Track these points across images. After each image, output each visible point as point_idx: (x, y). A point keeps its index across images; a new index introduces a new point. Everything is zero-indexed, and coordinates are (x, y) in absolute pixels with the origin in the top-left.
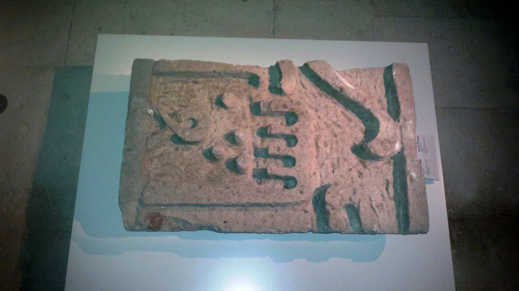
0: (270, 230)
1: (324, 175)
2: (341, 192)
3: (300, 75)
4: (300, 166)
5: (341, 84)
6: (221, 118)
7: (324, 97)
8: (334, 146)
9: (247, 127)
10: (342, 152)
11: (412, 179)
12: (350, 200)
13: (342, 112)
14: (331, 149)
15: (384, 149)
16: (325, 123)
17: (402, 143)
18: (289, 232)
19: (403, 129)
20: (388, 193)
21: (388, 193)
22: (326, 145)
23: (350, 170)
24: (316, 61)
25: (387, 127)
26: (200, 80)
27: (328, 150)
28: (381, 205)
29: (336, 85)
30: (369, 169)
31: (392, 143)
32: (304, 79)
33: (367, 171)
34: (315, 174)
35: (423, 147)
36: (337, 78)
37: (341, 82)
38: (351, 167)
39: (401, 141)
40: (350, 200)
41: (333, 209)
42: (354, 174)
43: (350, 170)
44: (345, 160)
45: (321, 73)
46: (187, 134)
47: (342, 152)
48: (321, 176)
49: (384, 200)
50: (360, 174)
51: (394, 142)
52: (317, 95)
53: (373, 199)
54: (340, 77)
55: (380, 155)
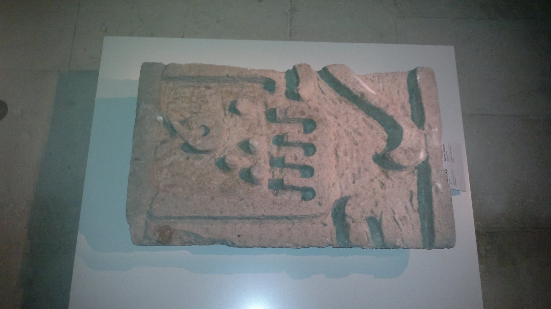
0: (287, 245)
1: (344, 186)
2: (362, 204)
3: (318, 79)
4: (319, 176)
5: (362, 89)
6: (235, 126)
7: (343, 102)
8: (355, 155)
10: (363, 161)
12: (372, 212)
13: (363, 119)
14: (351, 158)
15: (408, 158)
18: (306, 246)
19: (428, 137)
20: (412, 205)
22: (346, 154)
23: (372, 180)
24: (335, 65)
25: (411, 135)
26: (212, 85)
27: (348, 160)
28: (405, 217)
29: (356, 90)
30: (392, 179)
31: (416, 152)
33: (389, 181)
34: (334, 184)
35: (449, 156)
36: (358, 82)
37: (362, 87)
38: (373, 177)
39: (426, 149)
40: (372, 212)
41: (353, 222)
42: (376, 184)
44: (366, 169)
45: (341, 77)
46: (199, 142)
47: (363, 161)
48: (341, 187)
49: (407, 212)
50: (383, 185)
51: (419, 151)
52: (337, 101)
53: (396, 212)
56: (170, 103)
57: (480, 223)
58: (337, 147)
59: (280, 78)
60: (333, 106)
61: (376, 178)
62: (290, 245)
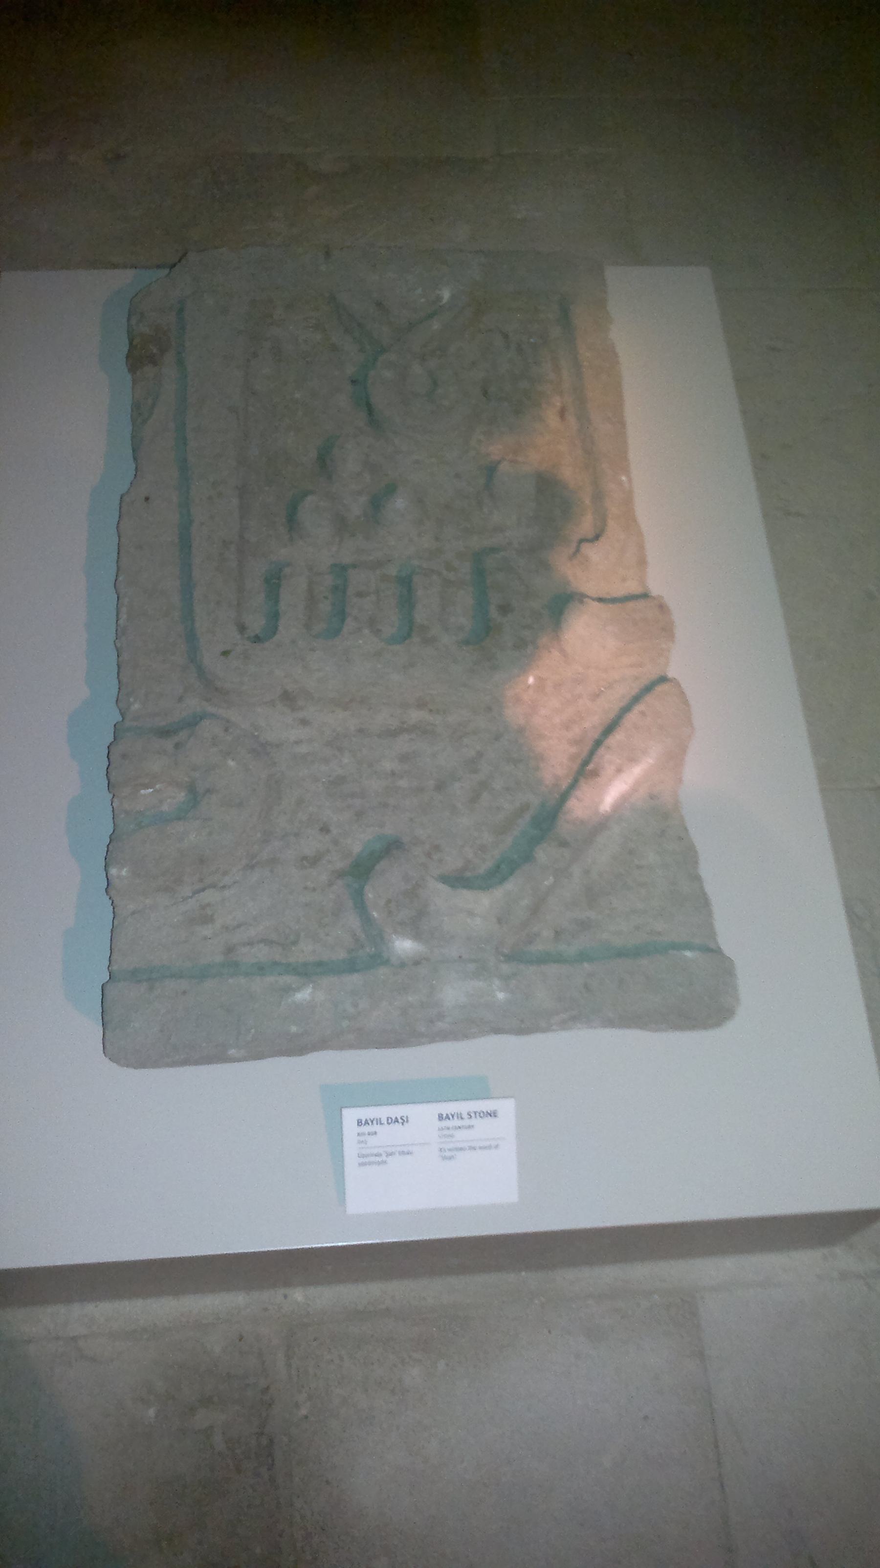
0: (124, 610)
1: (303, 749)
2: (231, 763)
3: (637, 678)
4: (313, 650)
5: (610, 770)
6: (457, 476)
7: (573, 750)
8: (403, 783)
9: (437, 539)
10: (385, 805)
11: (288, 990)
12: (208, 791)
13: (525, 808)
14: (393, 774)
15: (389, 901)
16: (480, 755)
17: (417, 963)
18: (121, 659)
19: (471, 967)
20: (250, 943)
21: (250, 943)
22: (404, 758)
23: (325, 829)
24: (686, 703)
25: (471, 914)
26: (572, 420)
27: (388, 766)
28: (207, 920)
29: (607, 758)
30: (330, 884)
31: (414, 927)
32: (651, 761)
33: (324, 878)
34: (304, 722)
35: (460, 1135)
36: (633, 760)
37: (619, 770)
38: (335, 831)
39: (427, 959)
40: (208, 791)
41: (177, 746)
42: (311, 843)
43: (325, 829)
44: (360, 814)
45: (643, 714)
46: (388, 374)
47: (385, 805)
48: (298, 742)
49: (226, 928)
50: (313, 861)
51: (417, 936)
52: (576, 730)
53: (227, 893)
54: (637, 771)
55: (367, 888)
56: (506, 336)
57: (304, 1411)
58: (424, 731)
59: (624, 580)
60: (557, 720)
61: (336, 842)
62: (124, 617)
